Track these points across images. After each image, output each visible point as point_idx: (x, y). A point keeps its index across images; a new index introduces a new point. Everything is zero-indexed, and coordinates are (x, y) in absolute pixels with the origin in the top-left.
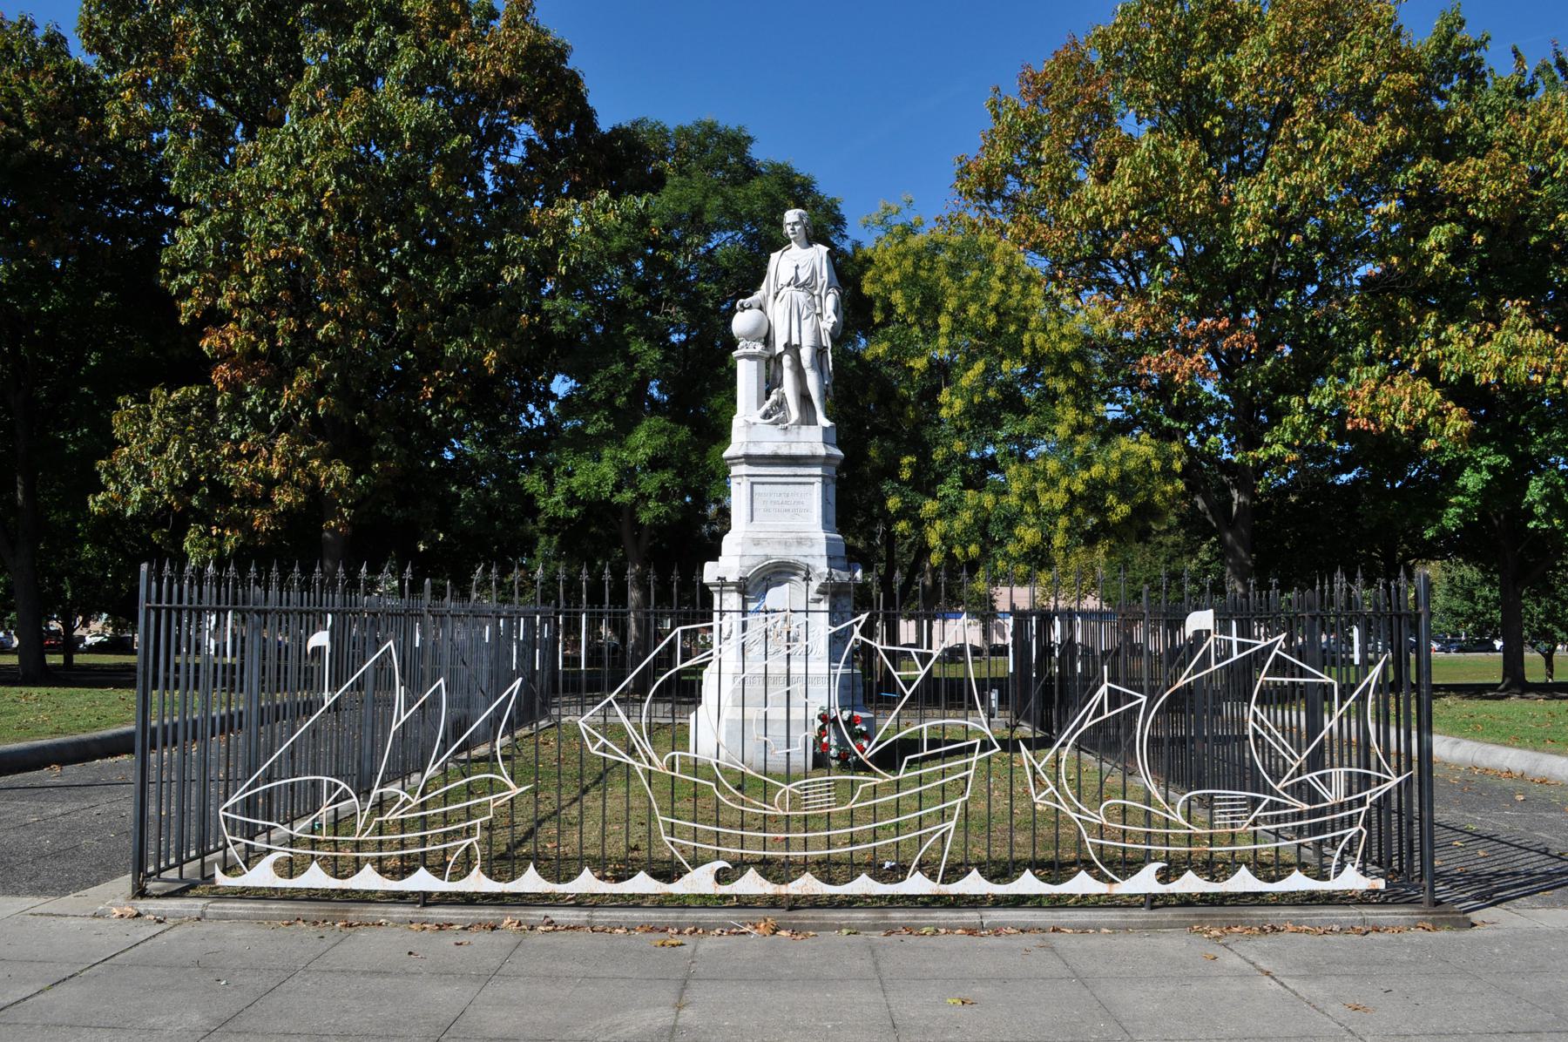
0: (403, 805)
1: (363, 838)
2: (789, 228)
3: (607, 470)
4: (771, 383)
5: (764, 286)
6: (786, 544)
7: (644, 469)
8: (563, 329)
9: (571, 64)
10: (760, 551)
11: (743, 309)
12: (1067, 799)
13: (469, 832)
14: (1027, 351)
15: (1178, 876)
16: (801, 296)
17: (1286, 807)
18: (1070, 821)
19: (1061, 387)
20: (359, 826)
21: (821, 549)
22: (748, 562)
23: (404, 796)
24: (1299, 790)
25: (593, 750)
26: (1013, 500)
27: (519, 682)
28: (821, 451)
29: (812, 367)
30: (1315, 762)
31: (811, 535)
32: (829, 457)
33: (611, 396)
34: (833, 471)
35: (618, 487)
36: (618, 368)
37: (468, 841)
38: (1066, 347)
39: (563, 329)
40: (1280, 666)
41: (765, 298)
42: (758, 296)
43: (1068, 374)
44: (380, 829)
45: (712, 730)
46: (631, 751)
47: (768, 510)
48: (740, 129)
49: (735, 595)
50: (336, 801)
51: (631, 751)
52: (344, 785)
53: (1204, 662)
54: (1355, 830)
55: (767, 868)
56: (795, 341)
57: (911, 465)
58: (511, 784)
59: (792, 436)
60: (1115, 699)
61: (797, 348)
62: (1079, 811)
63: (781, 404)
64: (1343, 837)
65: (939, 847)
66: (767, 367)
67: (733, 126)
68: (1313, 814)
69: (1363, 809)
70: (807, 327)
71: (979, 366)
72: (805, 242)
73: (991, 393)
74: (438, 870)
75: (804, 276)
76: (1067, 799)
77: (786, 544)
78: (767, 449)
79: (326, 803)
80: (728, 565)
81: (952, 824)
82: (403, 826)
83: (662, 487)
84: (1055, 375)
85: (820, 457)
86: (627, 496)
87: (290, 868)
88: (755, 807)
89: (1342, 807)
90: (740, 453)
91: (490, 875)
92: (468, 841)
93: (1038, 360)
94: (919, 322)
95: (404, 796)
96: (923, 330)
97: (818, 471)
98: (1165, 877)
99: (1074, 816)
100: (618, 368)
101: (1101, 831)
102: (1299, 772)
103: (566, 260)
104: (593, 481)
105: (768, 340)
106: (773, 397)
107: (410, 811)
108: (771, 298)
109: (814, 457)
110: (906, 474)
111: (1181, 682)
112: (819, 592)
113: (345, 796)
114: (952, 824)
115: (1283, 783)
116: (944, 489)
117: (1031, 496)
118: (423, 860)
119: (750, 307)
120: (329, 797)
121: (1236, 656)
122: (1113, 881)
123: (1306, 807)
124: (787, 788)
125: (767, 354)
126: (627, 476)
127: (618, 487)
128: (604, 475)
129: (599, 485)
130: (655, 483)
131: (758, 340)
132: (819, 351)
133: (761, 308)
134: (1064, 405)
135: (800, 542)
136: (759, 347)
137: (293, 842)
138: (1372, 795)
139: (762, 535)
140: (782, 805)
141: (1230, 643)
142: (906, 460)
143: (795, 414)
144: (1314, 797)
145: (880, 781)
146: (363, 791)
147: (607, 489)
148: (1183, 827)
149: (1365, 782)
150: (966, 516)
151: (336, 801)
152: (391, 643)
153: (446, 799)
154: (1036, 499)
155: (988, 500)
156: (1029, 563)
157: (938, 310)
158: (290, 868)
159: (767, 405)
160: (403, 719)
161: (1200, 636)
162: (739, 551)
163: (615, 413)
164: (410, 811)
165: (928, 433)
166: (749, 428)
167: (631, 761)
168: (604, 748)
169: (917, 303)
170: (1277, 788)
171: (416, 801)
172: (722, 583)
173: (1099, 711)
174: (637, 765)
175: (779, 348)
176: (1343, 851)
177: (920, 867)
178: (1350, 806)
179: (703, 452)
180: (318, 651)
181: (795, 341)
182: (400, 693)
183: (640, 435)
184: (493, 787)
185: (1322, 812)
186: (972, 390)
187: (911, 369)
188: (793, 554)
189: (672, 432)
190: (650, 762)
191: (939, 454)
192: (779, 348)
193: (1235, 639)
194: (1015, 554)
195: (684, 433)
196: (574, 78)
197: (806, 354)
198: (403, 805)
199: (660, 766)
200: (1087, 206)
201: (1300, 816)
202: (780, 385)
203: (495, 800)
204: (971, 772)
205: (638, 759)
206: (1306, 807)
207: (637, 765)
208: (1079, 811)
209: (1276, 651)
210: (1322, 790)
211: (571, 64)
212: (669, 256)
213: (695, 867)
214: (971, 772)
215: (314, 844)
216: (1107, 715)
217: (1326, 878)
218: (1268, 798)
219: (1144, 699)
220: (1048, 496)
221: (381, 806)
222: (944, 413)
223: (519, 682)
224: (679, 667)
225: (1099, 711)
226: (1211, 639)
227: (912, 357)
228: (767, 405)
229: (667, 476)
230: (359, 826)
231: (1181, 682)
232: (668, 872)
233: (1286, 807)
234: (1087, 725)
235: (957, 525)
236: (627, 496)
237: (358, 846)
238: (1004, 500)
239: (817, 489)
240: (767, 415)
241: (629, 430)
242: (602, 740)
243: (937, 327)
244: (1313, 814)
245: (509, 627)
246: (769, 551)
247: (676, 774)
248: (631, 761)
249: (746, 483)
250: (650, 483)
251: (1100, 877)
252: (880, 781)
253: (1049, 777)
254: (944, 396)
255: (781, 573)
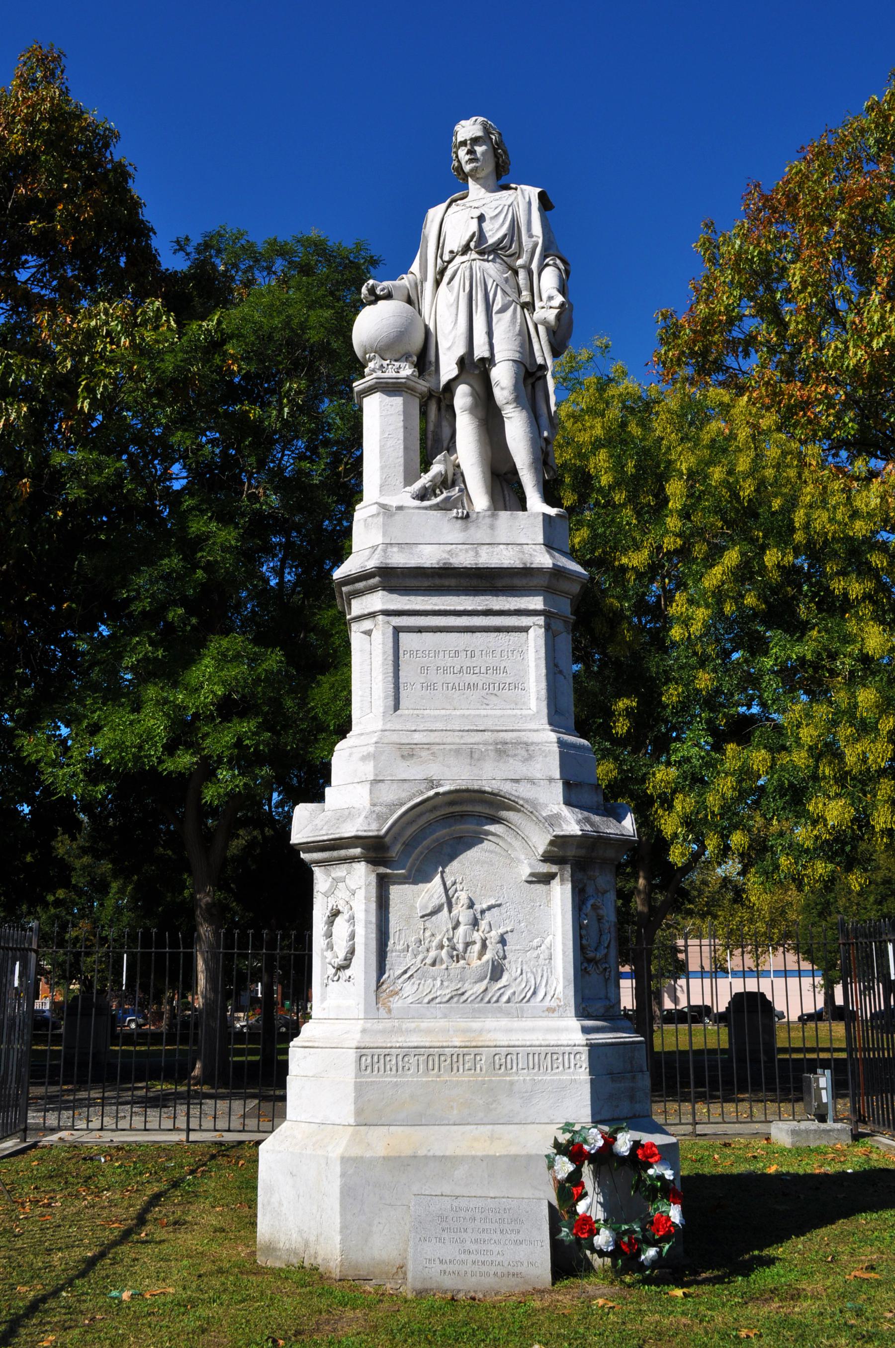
2: (462, 153)
3: (154, 722)
4: (430, 439)
5: (415, 267)
6: (472, 755)
7: (211, 718)
8: (81, 493)
9: (118, 153)
10: (415, 771)
11: (375, 298)
14: (799, 537)
16: (492, 270)
19: (856, 589)
21: (549, 764)
22: (389, 794)
26: (800, 758)
28: (544, 560)
29: (518, 400)
32: (557, 572)
33: (160, 609)
34: (565, 607)
35: (170, 749)
36: (172, 562)
38: (860, 528)
39: (81, 493)
41: (418, 286)
42: (405, 281)
43: (866, 571)
45: (313, 1175)
47: (431, 686)
48: (359, 247)
49: (361, 868)
56: (481, 351)
57: (629, 713)
59: (479, 533)
61: (488, 363)
63: (453, 479)
66: (424, 414)
67: (349, 244)
70: (505, 328)
71: (732, 557)
72: (492, 181)
73: (750, 600)
75: (494, 233)
77: (472, 755)
78: (428, 556)
80: (353, 795)
83: (239, 744)
84: (843, 573)
85: (540, 570)
86: (185, 760)
90: (372, 564)
93: (817, 551)
94: (632, 499)
96: (639, 514)
97: (537, 603)
100: (172, 562)
103: (90, 390)
104: (130, 739)
105: (424, 359)
106: (437, 468)
108: (429, 285)
109: (527, 572)
110: (621, 727)
112: (547, 858)
116: (684, 749)
117: (828, 751)
119: (389, 296)
125: (423, 386)
126: (183, 733)
127: (170, 749)
128: (149, 731)
129: (140, 748)
130: (228, 738)
131: (406, 357)
132: (530, 376)
133: (409, 301)
134: (860, 619)
135: (502, 750)
136: (407, 371)
139: (418, 738)
142: (622, 704)
143: (480, 500)
147: (154, 752)
150: (726, 785)
154: (839, 756)
155: (759, 758)
156: (830, 859)
157: (662, 478)
159: (425, 480)
162: (368, 770)
163: (168, 636)
165: (653, 664)
166: (389, 519)
169: (630, 467)
172: (334, 848)
175: (448, 370)
179: (302, 693)
181: (481, 351)
183: (207, 665)
186: (719, 596)
187: (623, 569)
188: (489, 776)
189: (254, 660)
191: (672, 695)
192: (448, 370)
194: (809, 844)
195: (274, 660)
196: (122, 173)
197: (502, 376)
200: (871, 336)
202: (451, 447)
211: (118, 153)
212: (254, 413)
220: (859, 748)
222: (676, 633)
227: (625, 551)
228: (425, 480)
229: (246, 727)
235: (712, 800)
236: (185, 760)
238: (784, 759)
239: (532, 647)
241: (190, 661)
243: (663, 501)
246: (434, 770)
249: (381, 630)
250: (220, 740)
254: (678, 606)
255: (462, 817)
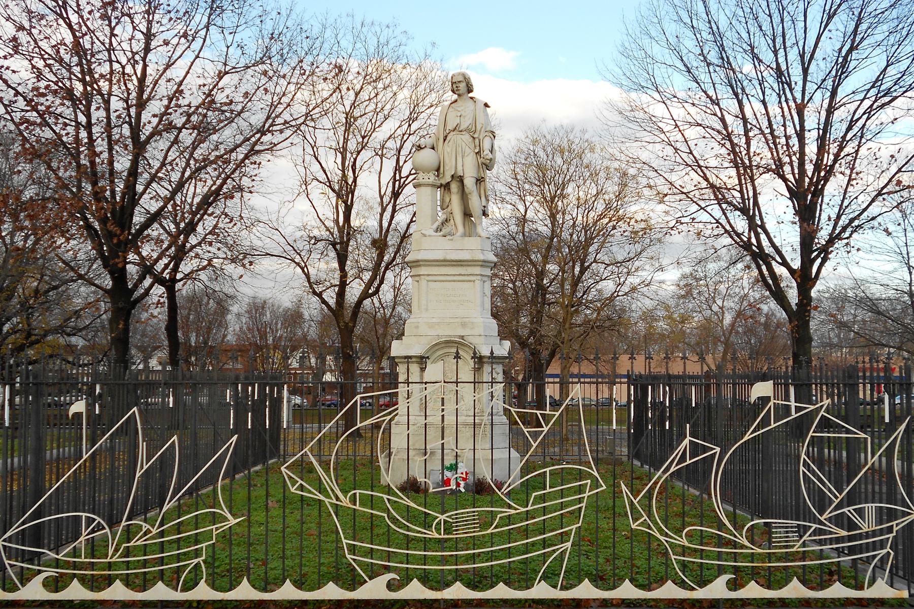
0: (145, 534)
1: (113, 560)
12: (656, 524)
13: (197, 553)
15: (742, 586)
17: (831, 533)
18: (660, 544)
20: (110, 554)
23: (148, 530)
24: (839, 521)
25: (293, 490)
27: (235, 438)
30: (851, 499)
31: (475, 320)
37: (196, 561)
40: (825, 424)
44: (128, 553)
46: (321, 490)
50: (93, 531)
51: (321, 490)
52: (98, 519)
53: (765, 422)
54: (884, 551)
55: (426, 579)
58: (229, 516)
60: (695, 449)
62: (667, 535)
64: (874, 557)
65: (558, 563)
68: (851, 538)
69: (891, 535)
74: (172, 584)
76: (656, 524)
79: (84, 534)
81: (569, 544)
82: (145, 550)
87: (55, 584)
88: (418, 531)
89: (874, 534)
91: (214, 587)
92: (196, 561)
95: (146, 526)
98: (734, 585)
99: (662, 538)
101: (684, 551)
102: (840, 506)
107: (152, 538)
111: (746, 438)
113: (100, 527)
114: (569, 544)
115: (826, 516)
118: (161, 576)
120: (87, 528)
121: (794, 415)
122: (693, 589)
123: (844, 533)
124: (442, 517)
133: (433, 148)
137: (57, 564)
138: (897, 525)
140: (438, 530)
141: (788, 407)
144: (852, 526)
145: (513, 512)
146: (113, 523)
148: (747, 548)
149: (892, 515)
151: (93, 531)
152: (233, 521)
153: (178, 529)
158: (55, 584)
160: (145, 467)
161: (765, 400)
164: (152, 538)
167: (322, 498)
168: (302, 488)
170: (822, 519)
171: (154, 531)
173: (683, 459)
174: (326, 500)
176: (875, 566)
177: (545, 578)
178: (881, 532)
180: (78, 415)
182: (142, 447)
184: (215, 518)
185: (860, 537)
190: (337, 499)
193: (793, 404)
198: (145, 534)
199: (345, 502)
201: (839, 540)
203: (217, 529)
204: (584, 505)
205: (328, 497)
206: (844, 533)
207: (326, 500)
208: (667, 535)
209: (822, 413)
210: (857, 520)
213: (370, 579)
214: (584, 505)
215: (75, 566)
216: (688, 462)
217: (861, 588)
218: (814, 526)
219: (718, 449)
221: (129, 534)
223: (235, 438)
224: (359, 425)
225: (683, 459)
226: (771, 404)
230: (110, 554)
231: (746, 438)
232: (354, 582)
233: (831, 533)
234: (672, 470)
237: (110, 566)
240: (438, 230)
242: (300, 482)
244: (851, 538)
245: (245, 390)
246: (441, 332)
247: (357, 507)
248: (322, 498)
251: (682, 585)
252: (513, 512)
253: (636, 508)
